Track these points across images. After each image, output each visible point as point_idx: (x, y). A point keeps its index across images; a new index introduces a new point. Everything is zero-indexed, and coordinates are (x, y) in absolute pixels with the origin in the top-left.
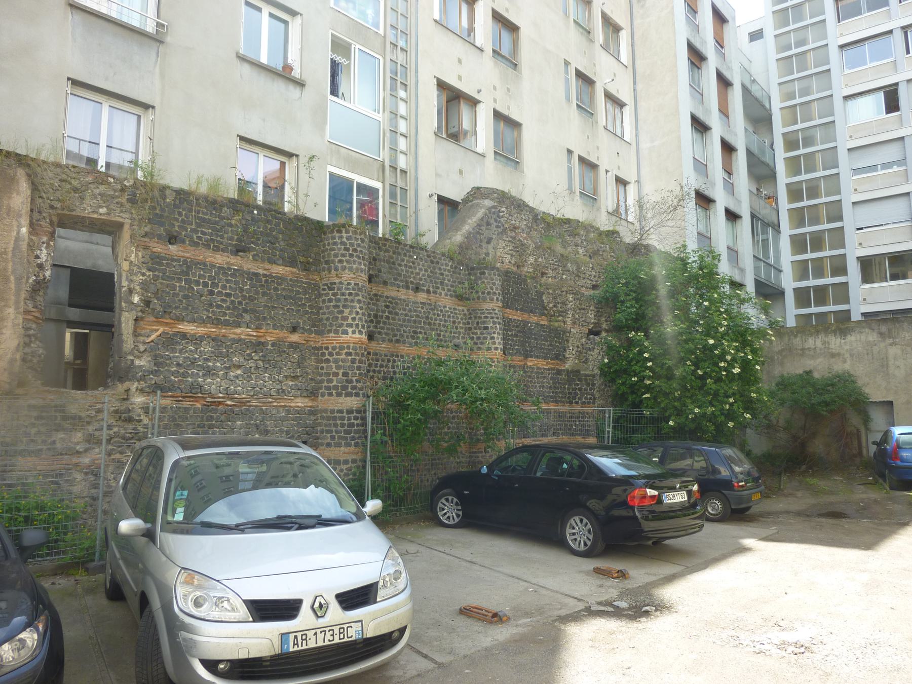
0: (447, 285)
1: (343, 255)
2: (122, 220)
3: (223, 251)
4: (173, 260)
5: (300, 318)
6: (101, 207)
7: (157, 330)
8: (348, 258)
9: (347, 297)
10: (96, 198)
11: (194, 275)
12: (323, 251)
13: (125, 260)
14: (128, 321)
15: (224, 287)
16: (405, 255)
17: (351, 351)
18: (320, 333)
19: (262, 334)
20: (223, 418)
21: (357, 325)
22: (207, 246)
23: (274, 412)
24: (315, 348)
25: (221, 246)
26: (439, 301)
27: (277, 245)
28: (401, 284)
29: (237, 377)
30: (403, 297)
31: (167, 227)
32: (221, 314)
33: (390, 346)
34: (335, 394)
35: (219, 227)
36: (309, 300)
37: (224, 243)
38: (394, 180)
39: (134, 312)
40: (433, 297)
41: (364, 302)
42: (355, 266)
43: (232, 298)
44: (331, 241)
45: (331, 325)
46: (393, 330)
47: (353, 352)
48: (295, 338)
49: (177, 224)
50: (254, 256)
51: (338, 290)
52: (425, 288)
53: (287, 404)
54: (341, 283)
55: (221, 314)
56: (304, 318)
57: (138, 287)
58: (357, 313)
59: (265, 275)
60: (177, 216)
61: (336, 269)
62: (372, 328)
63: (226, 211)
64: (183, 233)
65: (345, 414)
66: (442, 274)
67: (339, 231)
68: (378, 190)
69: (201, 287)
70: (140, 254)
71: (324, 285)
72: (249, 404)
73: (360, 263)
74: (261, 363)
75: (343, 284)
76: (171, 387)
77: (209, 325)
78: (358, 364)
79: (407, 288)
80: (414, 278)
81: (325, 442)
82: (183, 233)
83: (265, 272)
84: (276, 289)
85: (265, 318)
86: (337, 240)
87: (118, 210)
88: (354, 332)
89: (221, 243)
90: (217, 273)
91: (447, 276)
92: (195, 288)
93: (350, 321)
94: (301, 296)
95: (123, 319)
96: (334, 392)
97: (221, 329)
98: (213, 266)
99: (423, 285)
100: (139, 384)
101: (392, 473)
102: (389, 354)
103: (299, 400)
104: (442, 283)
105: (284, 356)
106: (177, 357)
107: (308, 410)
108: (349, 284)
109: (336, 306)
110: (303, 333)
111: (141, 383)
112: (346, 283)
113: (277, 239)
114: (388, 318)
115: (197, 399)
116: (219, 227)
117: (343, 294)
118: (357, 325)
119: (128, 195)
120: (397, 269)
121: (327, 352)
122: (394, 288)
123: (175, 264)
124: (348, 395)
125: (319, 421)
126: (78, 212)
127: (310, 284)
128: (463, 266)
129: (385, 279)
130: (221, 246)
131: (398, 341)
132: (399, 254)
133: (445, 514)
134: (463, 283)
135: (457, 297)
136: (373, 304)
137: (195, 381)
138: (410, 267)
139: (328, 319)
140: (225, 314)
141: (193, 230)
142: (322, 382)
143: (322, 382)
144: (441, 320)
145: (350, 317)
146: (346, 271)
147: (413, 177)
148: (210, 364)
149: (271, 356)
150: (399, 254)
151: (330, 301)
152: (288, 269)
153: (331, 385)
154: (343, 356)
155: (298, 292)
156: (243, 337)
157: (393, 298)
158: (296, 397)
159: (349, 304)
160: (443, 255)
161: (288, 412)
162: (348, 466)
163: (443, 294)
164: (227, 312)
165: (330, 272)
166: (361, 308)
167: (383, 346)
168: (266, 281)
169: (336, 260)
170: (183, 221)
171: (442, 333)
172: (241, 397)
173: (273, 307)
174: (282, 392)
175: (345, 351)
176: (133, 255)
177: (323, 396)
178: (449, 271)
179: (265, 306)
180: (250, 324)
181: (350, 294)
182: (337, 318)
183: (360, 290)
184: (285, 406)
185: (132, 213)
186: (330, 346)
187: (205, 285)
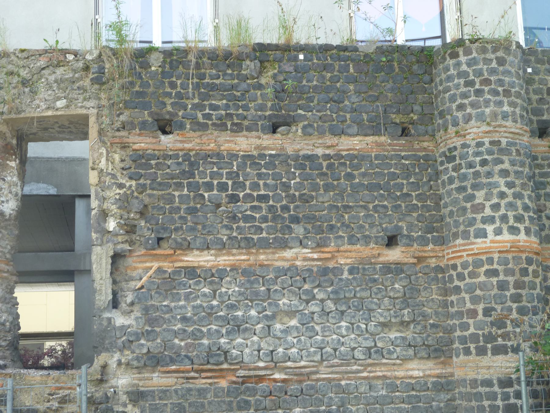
1: (465, 96)
2: (84, 111)
3: (249, 129)
4: (167, 157)
5: (400, 220)
6: (59, 99)
7: (151, 268)
8: (473, 98)
9: (478, 168)
10: (51, 87)
11: (203, 174)
13: (93, 169)
14: (101, 259)
15: (255, 186)
17: (495, 266)
19: (329, 256)
21: (504, 218)
22: (221, 126)
25: (246, 123)
27: (347, 103)
31: (154, 109)
32: (253, 230)
34: (474, 351)
35: (239, 94)
37: (249, 117)
39: (110, 245)
42: (488, 111)
43: (271, 203)
44: (443, 76)
45: (457, 224)
47: (500, 268)
49: (169, 101)
51: (461, 159)
53: (389, 374)
54: (464, 146)
55: (253, 230)
56: (408, 219)
57: (114, 207)
58: (502, 195)
59: (327, 157)
60: (169, 90)
61: (456, 124)
64: (180, 114)
65: (496, 389)
67: (454, 55)
69: (215, 192)
70: (117, 157)
72: (314, 377)
73: (500, 104)
74: (330, 305)
75: (468, 146)
76: (174, 356)
77: (234, 251)
78: (513, 291)
82: (180, 114)
83: (327, 152)
84: (350, 177)
85: (332, 228)
86: (452, 72)
87: (81, 97)
88: (499, 232)
89: (245, 118)
92: (206, 195)
93: (488, 212)
94: (399, 181)
95: (94, 257)
96: (472, 346)
97: (257, 253)
98: (233, 156)
100: (122, 354)
103: (413, 365)
105: (374, 290)
106: (181, 307)
107: (433, 383)
108: (480, 144)
109: (461, 189)
111: (127, 352)
112: (473, 143)
115: (224, 373)
116: (239, 94)
117: (471, 165)
118: (504, 218)
119: (93, 73)
121: (454, 273)
123: (169, 162)
124: (499, 350)
126: (30, 113)
127: (418, 158)
130: (246, 123)
137: (214, 344)
139: (451, 213)
141: (196, 107)
142: (452, 330)
145: (488, 204)
146: (473, 122)
148: (240, 313)
151: (451, 180)
152: (370, 139)
153: (467, 333)
154: (482, 278)
158: (406, 360)
159: (484, 180)
161: (393, 387)
164: (263, 225)
165: (446, 130)
166: (510, 185)
168: (330, 166)
169: (454, 106)
170: (179, 96)
172: (298, 365)
173: (346, 207)
174: (376, 352)
175: (484, 269)
176: (103, 160)
179: (331, 207)
180: (305, 241)
181: (484, 163)
182: (464, 209)
184: (385, 377)
185: (100, 99)
186: (458, 262)
187: (223, 187)
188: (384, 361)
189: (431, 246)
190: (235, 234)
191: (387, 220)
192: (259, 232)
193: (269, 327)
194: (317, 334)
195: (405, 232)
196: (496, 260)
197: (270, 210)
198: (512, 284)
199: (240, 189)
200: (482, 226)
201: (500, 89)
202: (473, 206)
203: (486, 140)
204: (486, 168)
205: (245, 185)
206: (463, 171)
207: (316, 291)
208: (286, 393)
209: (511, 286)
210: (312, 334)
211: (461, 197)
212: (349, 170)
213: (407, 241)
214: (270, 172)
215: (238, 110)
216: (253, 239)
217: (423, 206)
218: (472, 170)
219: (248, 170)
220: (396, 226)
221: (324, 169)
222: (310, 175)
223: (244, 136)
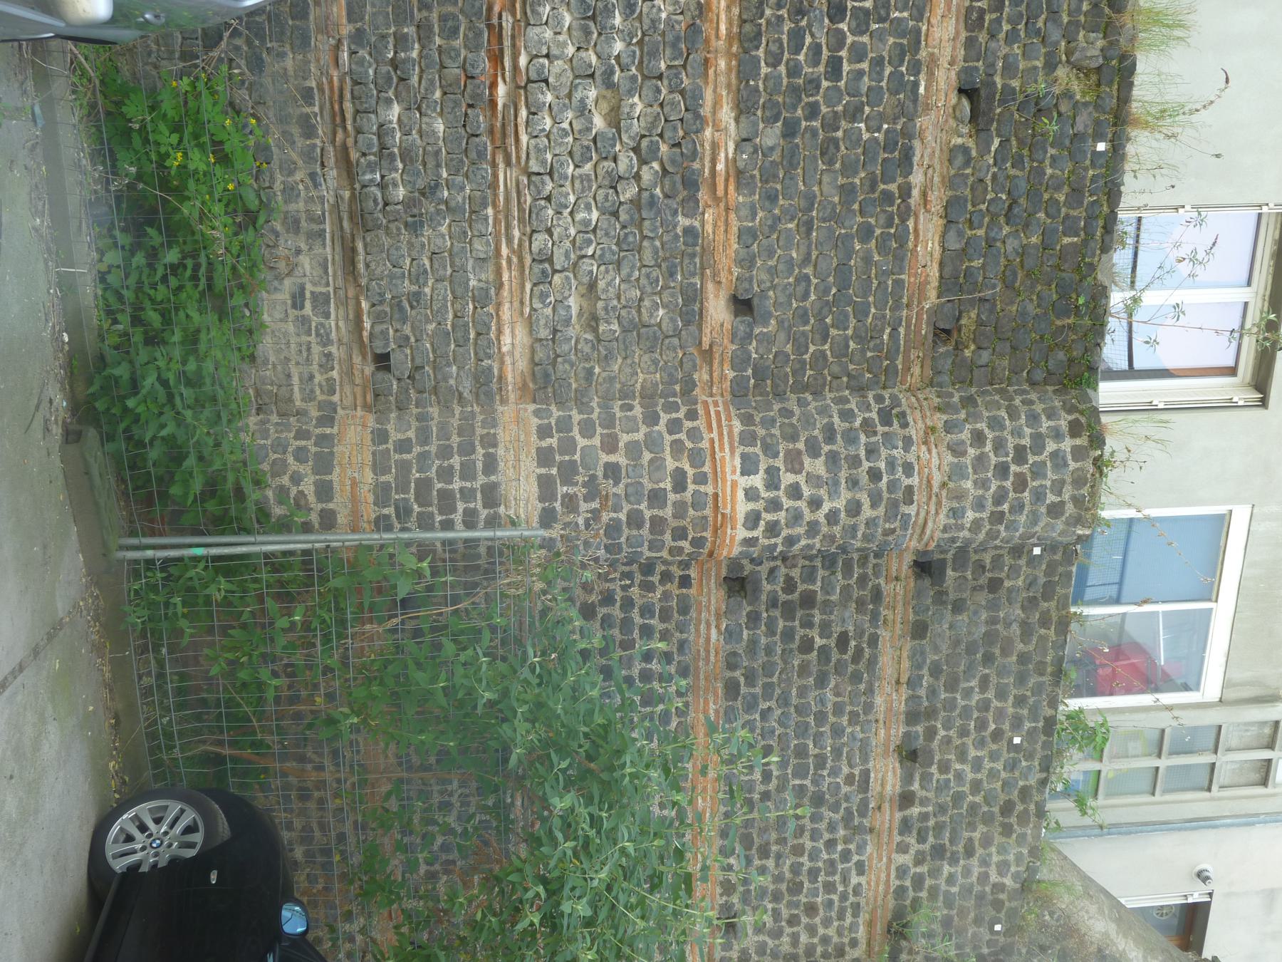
0: (934, 873)
1: (999, 445)
3: (970, 43)
5: (780, 323)
8: (993, 460)
9: (866, 465)
12: (1002, 392)
16: (1020, 701)
17: (691, 487)
18: (739, 393)
19: (720, 192)
20: (454, 71)
23: (478, 245)
24: (689, 386)
25: (982, 37)
26: (879, 846)
27: (1006, 230)
28: (922, 692)
29: (583, 111)
30: (879, 700)
32: (774, 48)
33: (715, 661)
34: (544, 444)
35: (1040, 24)
36: (842, 351)
37: (993, 45)
38: (1234, 742)
40: (888, 818)
41: (854, 528)
42: (969, 484)
43: (825, 84)
44: (1039, 407)
46: (768, 669)
47: (688, 495)
48: (718, 310)
50: (965, 150)
51: (885, 434)
52: (916, 786)
53: (505, 293)
54: (908, 442)
55: (774, 48)
56: (782, 336)
58: (815, 504)
59: (906, 191)
61: (949, 427)
62: (767, 587)
63: (1092, 46)
65: (481, 479)
66: (969, 852)
67: (1075, 430)
68: (1197, 687)
71: (894, 398)
72: (500, 159)
73: (979, 505)
75: (906, 449)
78: (648, 514)
79: (912, 717)
80: (947, 741)
81: (390, 427)
85: (772, 198)
86: (1046, 424)
88: (751, 494)
89: (993, 36)
90: (898, 28)
91: (967, 872)
93: (787, 479)
94: (852, 322)
96: (553, 441)
99: (926, 778)
101: (283, 623)
102: (687, 658)
104: (938, 852)
107: (490, 368)
108: (908, 470)
109: (830, 434)
110: (734, 336)
112: (911, 458)
113: (1027, 226)
114: (807, 646)
116: (1040, 24)
117: (871, 452)
118: (774, 505)
120: (969, 672)
121: (681, 415)
122: (906, 664)
125: (458, 410)
127: (891, 356)
128: (1007, 932)
129: (934, 628)
130: (982, 37)
131: (732, 689)
132: (1021, 679)
133: (143, 828)
134: (947, 935)
135: (899, 914)
136: (846, 590)
138: (982, 725)
139: (787, 413)
140: (774, 61)
142: (583, 406)
143: (583, 406)
144: (814, 856)
145: (801, 479)
146: (949, 458)
147: (1252, 806)
148: (618, 20)
149: (654, 230)
150: (1021, 679)
151: (847, 415)
152: (934, 272)
153: (576, 432)
154: (671, 464)
155: (861, 312)
156: (708, 132)
157: (873, 662)
158: (531, 323)
159: (843, 475)
160: (1035, 852)
161: (482, 299)
162: (312, 499)
163: (901, 859)
164: (782, 69)
166: (832, 517)
167: (714, 632)
168: (887, 197)
169: (982, 426)
171: (770, 863)
172: (522, 129)
173: (809, 226)
174: (543, 272)
175: (687, 467)
177: (537, 413)
178: (984, 877)
179: (810, 199)
180: (748, 147)
181: (875, 475)
182: (794, 438)
183: (893, 505)
184: (500, 286)
186: (700, 423)
188: (528, 286)
189: (730, 374)
190: (768, 12)
191: (781, 300)
192: (770, 60)
193: (592, 76)
194: (576, 166)
195: (757, 331)
196: (702, 488)
197: (811, 81)
198: (661, 513)
199: (854, 24)
200: (762, 467)
201: (1006, 507)
202: (799, 452)
203: (915, 481)
204: (864, 479)
205: (862, 33)
206: (863, 438)
207: (656, 165)
208: (470, 106)
209: (656, 512)
210: (577, 157)
211: (816, 432)
212: (878, 232)
213: (741, 334)
214: (884, 84)
215: (1008, 22)
216: (757, 48)
217: (803, 362)
218: (863, 453)
219: (891, 40)
220: (770, 315)
221: (882, 187)
222: (874, 159)
223: (957, 33)
